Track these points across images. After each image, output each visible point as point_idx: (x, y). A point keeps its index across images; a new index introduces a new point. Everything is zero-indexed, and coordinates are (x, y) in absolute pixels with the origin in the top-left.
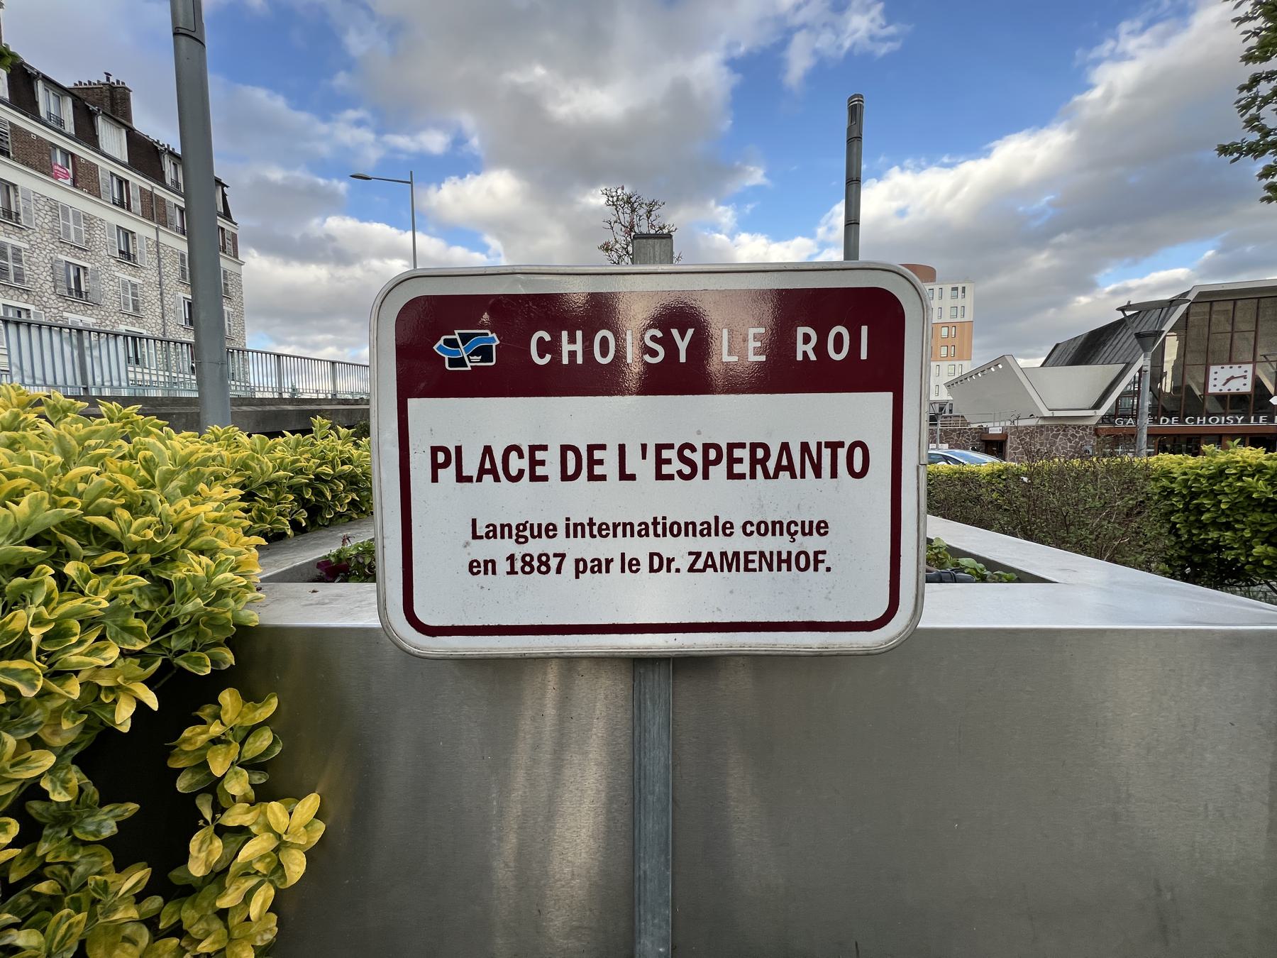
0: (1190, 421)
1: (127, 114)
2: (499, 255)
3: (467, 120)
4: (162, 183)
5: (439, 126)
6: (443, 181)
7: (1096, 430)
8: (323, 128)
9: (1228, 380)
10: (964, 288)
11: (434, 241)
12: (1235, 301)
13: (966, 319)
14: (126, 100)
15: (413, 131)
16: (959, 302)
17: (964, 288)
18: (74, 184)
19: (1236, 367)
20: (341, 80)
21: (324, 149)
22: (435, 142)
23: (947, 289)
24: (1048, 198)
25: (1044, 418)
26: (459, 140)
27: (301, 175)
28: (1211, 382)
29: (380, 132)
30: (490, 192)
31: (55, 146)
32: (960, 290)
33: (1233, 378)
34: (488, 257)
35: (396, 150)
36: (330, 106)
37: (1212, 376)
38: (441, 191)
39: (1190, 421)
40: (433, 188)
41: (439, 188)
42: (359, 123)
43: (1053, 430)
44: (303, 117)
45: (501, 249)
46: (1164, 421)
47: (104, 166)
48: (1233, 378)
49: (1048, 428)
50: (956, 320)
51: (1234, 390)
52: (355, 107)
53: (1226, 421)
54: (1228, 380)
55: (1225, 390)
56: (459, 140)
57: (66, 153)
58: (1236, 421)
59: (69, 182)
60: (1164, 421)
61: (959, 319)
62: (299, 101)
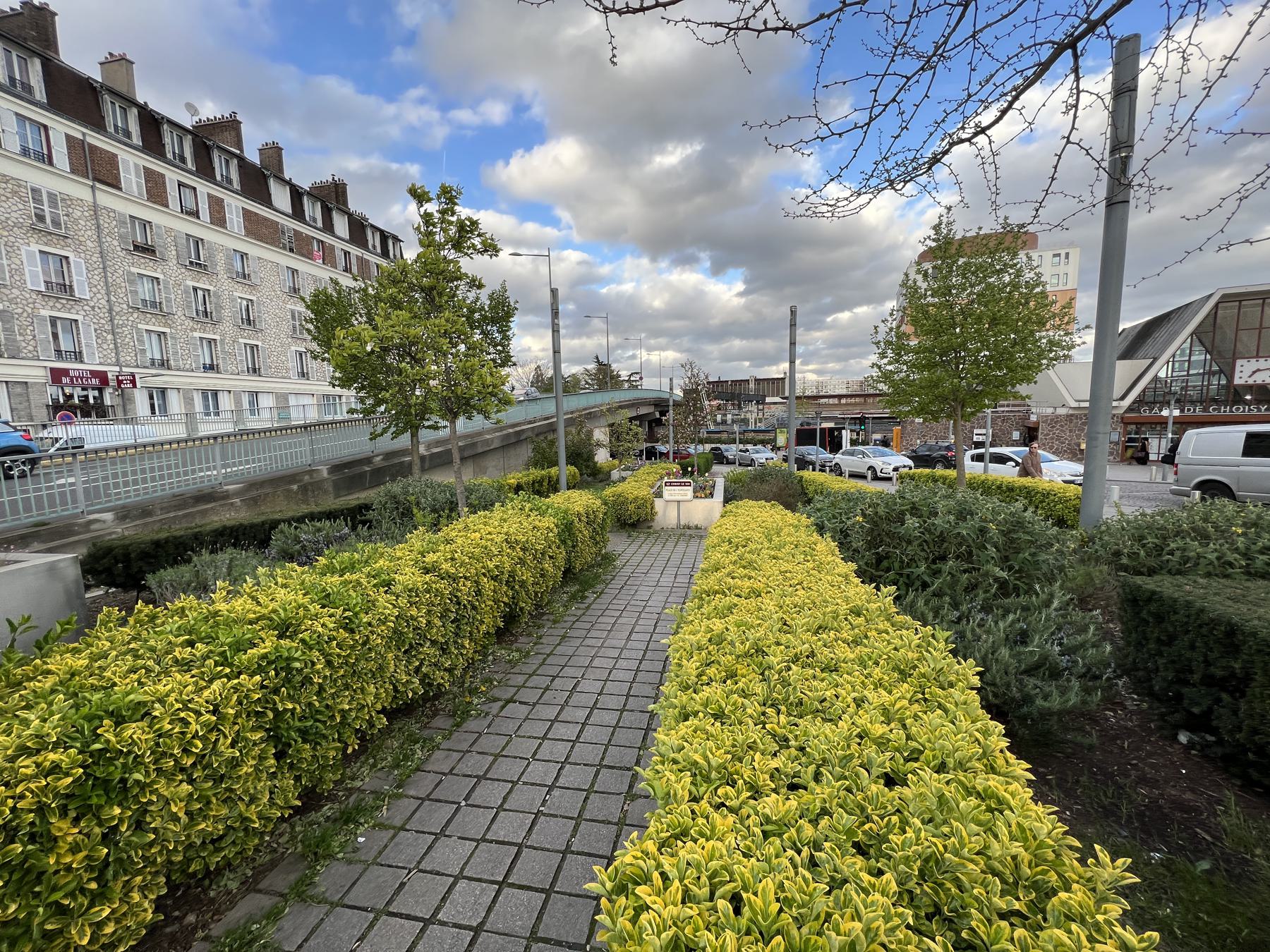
0: (1214, 410)
1: (345, 203)
2: (570, 228)
3: (527, 85)
4: (368, 250)
5: (495, 93)
6: (510, 156)
7: (1122, 418)
8: (391, 109)
9: (1254, 372)
10: (1067, 255)
11: (505, 217)
12: (1264, 299)
13: (1069, 287)
14: (344, 192)
15: (474, 105)
16: (1062, 269)
17: (1067, 255)
18: (324, 263)
19: (1262, 360)
20: (400, 56)
21: (395, 132)
22: (496, 112)
23: (1048, 255)
24: (1234, 97)
25: (1074, 408)
26: (520, 107)
27: (375, 161)
28: (1237, 375)
29: (446, 106)
30: (556, 160)
31: (314, 238)
32: (1063, 256)
33: (1258, 370)
34: (560, 230)
35: (462, 127)
36: (392, 87)
37: (1238, 368)
38: (510, 166)
39: (1214, 410)
40: (500, 164)
41: (507, 163)
42: (422, 101)
43: (1081, 419)
44: (370, 102)
45: (572, 222)
46: (1189, 410)
47: (339, 245)
48: (1258, 370)
49: (1077, 417)
50: (1056, 289)
51: (1259, 382)
52: (414, 85)
53: (1250, 410)
54: (1254, 372)
55: (1251, 381)
56: (520, 107)
57: (320, 242)
58: (1259, 410)
59: (321, 261)
60: (1189, 410)
61: (1061, 287)
62: (366, 85)
